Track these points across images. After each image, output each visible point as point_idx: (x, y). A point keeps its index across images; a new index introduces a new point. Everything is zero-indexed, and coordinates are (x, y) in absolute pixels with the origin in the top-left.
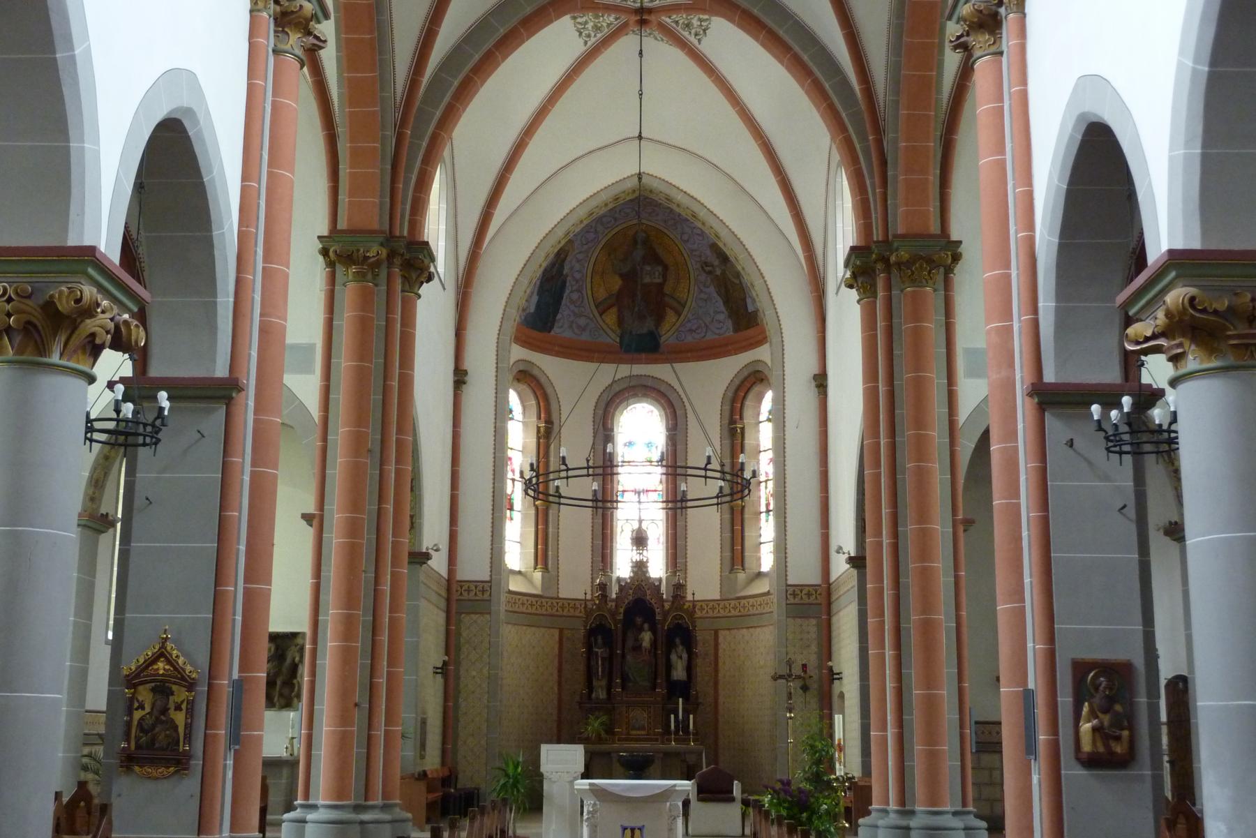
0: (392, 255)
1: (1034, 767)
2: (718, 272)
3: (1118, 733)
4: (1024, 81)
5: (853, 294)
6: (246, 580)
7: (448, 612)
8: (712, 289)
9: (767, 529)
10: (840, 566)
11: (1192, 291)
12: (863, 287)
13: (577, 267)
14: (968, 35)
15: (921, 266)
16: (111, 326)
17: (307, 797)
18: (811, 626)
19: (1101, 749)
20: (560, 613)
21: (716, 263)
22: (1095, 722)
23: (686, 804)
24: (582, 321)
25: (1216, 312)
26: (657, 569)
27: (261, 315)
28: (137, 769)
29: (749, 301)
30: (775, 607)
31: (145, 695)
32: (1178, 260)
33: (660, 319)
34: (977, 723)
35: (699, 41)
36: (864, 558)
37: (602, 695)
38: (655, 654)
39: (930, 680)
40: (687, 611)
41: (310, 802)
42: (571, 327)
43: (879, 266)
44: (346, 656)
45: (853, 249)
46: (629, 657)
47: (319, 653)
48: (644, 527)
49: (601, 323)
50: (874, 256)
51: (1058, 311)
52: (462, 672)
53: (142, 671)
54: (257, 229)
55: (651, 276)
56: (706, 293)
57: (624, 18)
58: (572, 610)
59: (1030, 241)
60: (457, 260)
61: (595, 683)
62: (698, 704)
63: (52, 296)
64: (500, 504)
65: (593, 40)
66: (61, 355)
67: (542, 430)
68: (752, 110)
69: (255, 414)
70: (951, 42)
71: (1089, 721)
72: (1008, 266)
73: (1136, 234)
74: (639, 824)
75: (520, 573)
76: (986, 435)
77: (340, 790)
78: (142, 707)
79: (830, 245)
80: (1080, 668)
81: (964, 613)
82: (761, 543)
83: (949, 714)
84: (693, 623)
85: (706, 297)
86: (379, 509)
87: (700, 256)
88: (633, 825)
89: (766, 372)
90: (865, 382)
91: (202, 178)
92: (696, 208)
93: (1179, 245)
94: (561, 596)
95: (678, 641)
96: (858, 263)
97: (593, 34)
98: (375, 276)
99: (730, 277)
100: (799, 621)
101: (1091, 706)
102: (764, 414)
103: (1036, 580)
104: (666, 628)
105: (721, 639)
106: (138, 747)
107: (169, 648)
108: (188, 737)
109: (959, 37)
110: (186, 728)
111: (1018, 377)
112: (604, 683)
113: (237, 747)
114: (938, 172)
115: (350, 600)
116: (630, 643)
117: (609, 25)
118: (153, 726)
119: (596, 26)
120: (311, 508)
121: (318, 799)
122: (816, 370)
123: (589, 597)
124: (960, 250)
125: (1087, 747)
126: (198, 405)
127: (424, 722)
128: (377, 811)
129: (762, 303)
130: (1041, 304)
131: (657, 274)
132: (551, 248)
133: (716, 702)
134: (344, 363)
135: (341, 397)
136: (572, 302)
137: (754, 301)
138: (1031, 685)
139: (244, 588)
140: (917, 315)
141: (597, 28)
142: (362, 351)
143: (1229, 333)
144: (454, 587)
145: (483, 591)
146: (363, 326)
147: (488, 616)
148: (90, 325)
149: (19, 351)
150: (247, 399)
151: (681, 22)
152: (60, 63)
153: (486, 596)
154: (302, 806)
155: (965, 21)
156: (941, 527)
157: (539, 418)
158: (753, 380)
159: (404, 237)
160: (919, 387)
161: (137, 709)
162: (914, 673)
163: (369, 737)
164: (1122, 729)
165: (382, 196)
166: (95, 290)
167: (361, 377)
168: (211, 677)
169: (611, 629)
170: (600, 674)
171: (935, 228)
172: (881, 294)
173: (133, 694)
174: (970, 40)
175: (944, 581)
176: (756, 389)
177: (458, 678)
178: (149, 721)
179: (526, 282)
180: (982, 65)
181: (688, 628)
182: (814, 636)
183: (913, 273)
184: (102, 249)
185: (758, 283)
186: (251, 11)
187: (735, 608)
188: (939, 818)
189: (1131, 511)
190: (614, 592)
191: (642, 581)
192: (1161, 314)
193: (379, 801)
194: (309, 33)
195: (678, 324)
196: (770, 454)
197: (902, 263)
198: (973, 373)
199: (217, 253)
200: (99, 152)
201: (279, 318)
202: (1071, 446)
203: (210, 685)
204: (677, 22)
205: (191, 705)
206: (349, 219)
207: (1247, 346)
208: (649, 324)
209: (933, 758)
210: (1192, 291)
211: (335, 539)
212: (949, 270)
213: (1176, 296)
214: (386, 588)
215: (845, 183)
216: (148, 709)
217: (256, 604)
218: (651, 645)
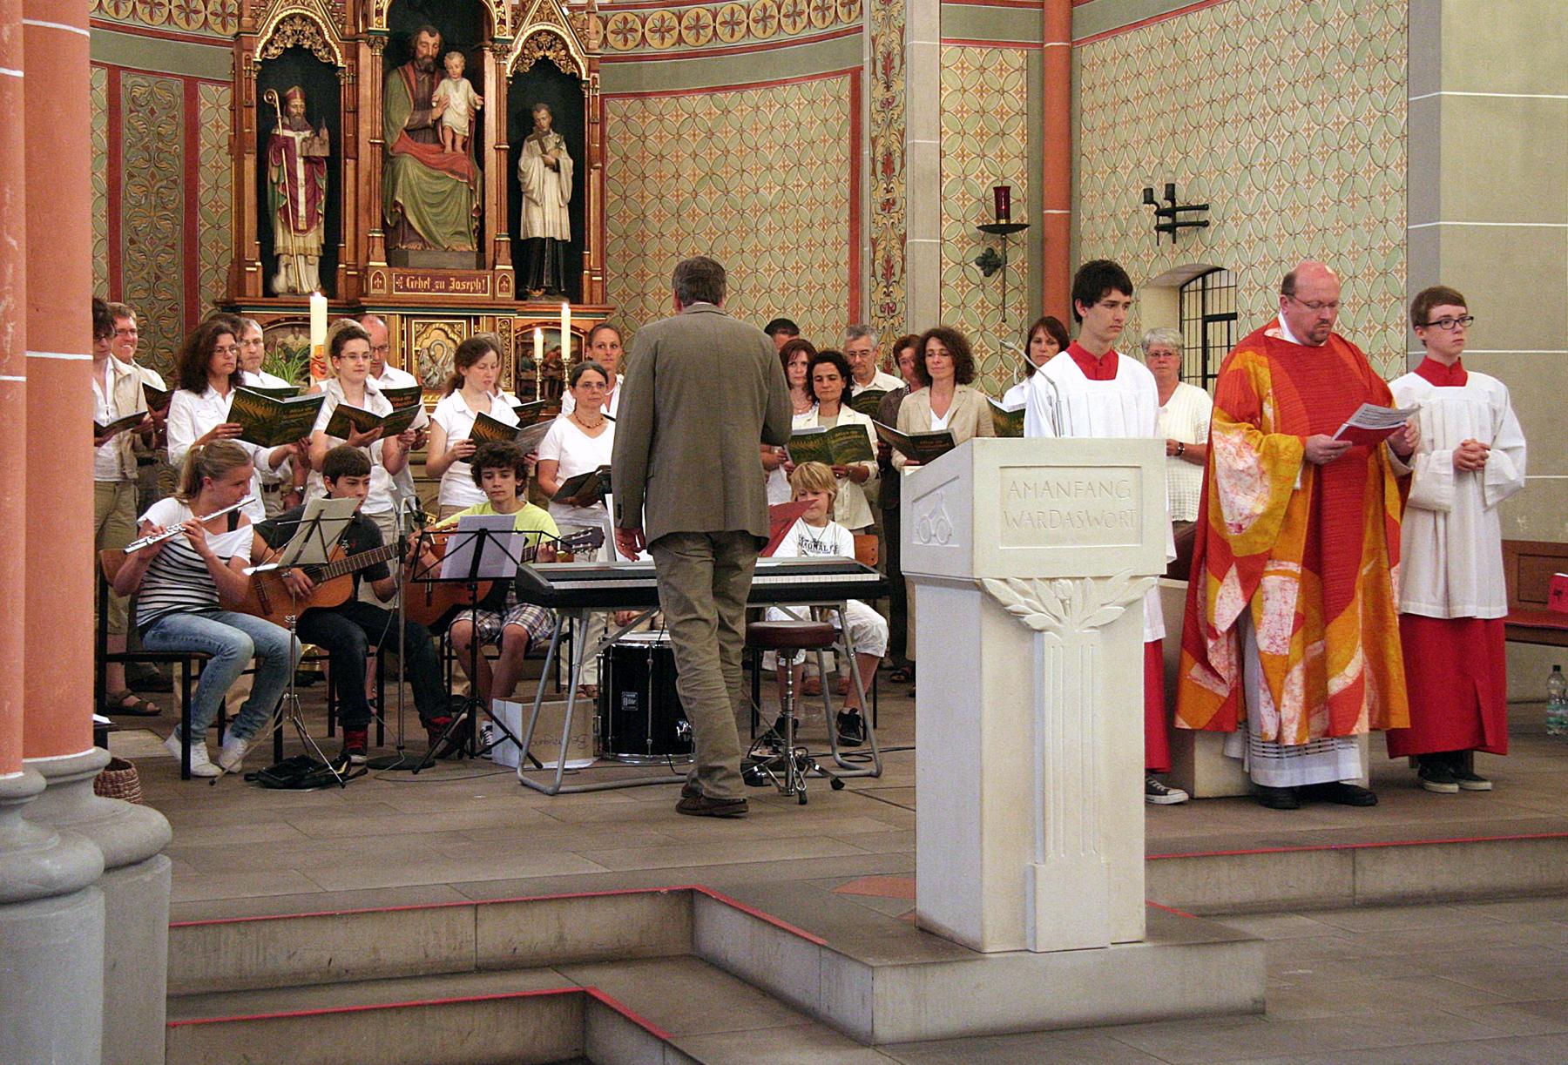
61: (282, 239)
95: (543, 116)
112: (313, 240)
182: (1015, 102)
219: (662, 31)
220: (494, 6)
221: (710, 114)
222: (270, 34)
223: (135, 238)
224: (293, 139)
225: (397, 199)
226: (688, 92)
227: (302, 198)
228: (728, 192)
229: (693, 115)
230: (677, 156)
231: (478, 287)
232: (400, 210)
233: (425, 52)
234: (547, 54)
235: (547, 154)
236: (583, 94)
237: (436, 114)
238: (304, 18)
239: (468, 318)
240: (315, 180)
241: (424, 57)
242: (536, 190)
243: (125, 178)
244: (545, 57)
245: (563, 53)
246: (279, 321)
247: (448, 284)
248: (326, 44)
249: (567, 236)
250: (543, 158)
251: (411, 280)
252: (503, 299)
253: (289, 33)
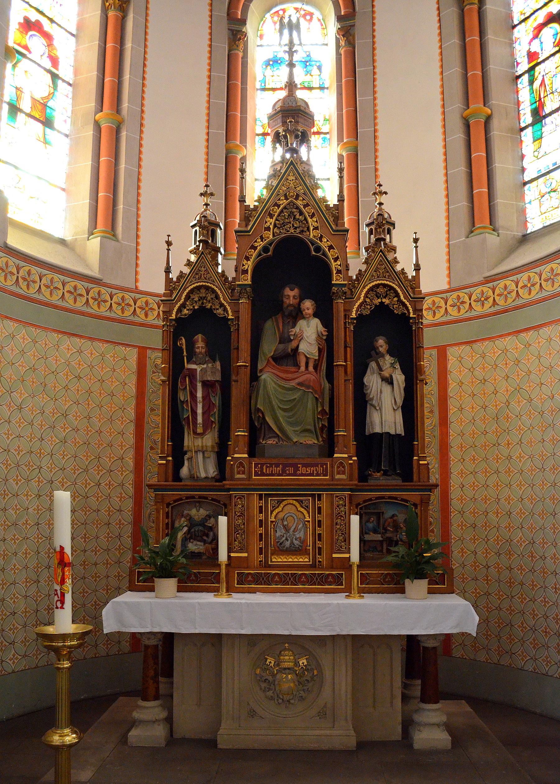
61: (188, 441)
75: (62, 242)
82: (525, 184)
84: (418, 311)
94: (142, 287)
95: (381, 343)
104: (354, 315)
169: (226, 319)
170: (200, 419)
181: (405, 318)
191: (297, 198)
218: (320, 350)
219: (482, 301)
220: (332, 261)
221: (517, 348)
222: (183, 300)
223: (154, 446)
224: (196, 370)
225: (258, 406)
226: (501, 336)
227: (200, 411)
228: (532, 400)
229: (505, 351)
230: (495, 380)
231: (320, 470)
232: (261, 415)
233: (288, 302)
234: (384, 300)
235: (382, 371)
236: (411, 327)
237: (294, 344)
238: (207, 288)
239: (313, 496)
240: (210, 398)
241: (288, 306)
242: (375, 398)
243: (148, 411)
244: (382, 303)
245: (396, 299)
246: (181, 499)
247: (296, 469)
248: (222, 305)
249: (400, 430)
250: (380, 374)
251: (267, 467)
252: (339, 480)
253: (196, 299)
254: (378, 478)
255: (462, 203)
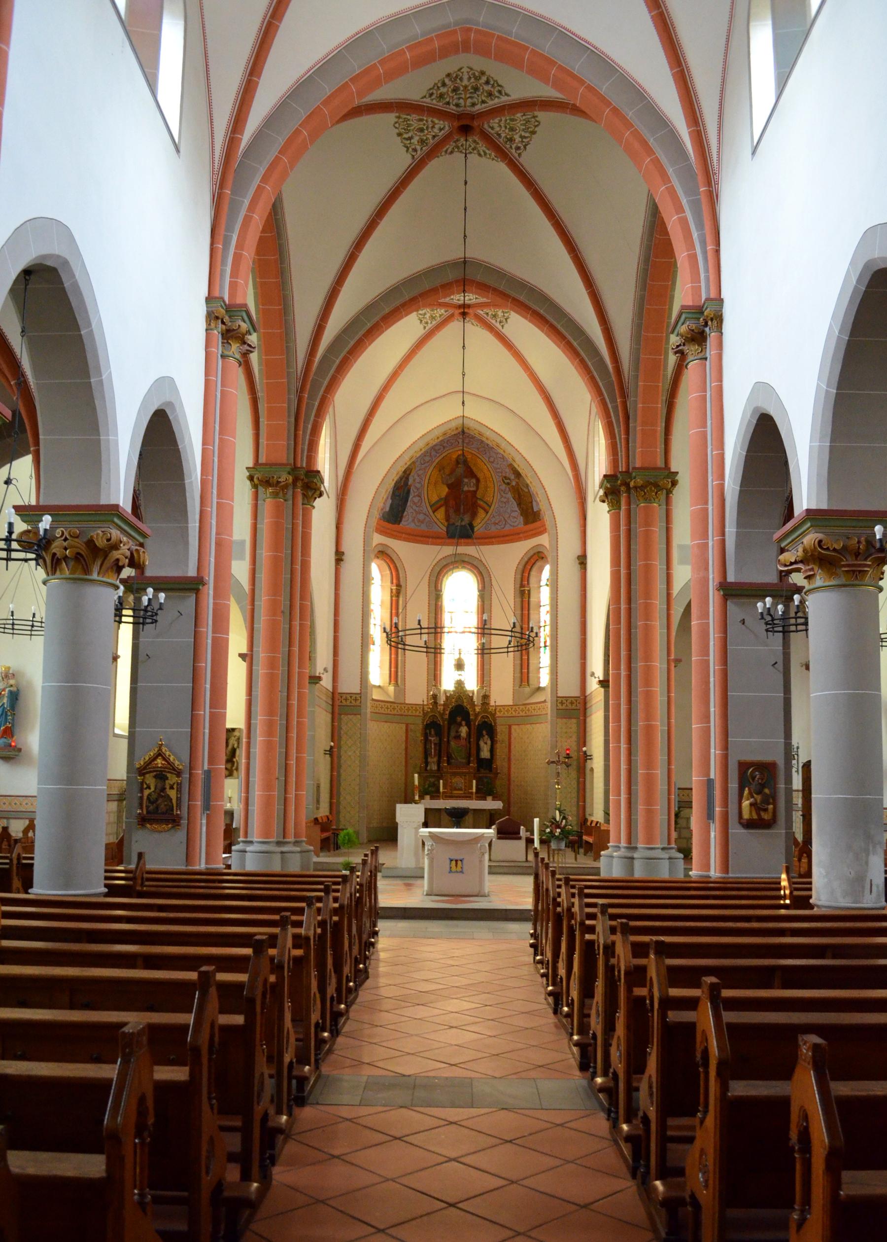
0: (295, 480)
1: (712, 826)
2: (514, 483)
3: (766, 807)
4: (720, 379)
5: (605, 507)
6: (211, 707)
7: (333, 713)
8: (509, 495)
9: (545, 658)
10: (593, 686)
11: (820, 536)
12: (612, 502)
13: (418, 480)
14: (684, 345)
15: (651, 489)
16: (128, 554)
17: (246, 835)
18: (573, 724)
19: (755, 817)
20: (406, 713)
21: (512, 477)
22: (752, 800)
23: (490, 845)
24: (421, 517)
25: (835, 550)
26: (472, 684)
27: (217, 534)
28: (148, 826)
29: (534, 503)
30: (548, 709)
31: (150, 780)
32: (810, 513)
33: (474, 515)
34: (679, 789)
35: (503, 326)
36: (608, 681)
37: (435, 767)
38: (470, 742)
39: (650, 764)
40: (491, 713)
41: (248, 839)
42: (413, 520)
43: (623, 488)
44: (269, 746)
45: (605, 476)
46: (452, 743)
47: (251, 745)
48: (462, 657)
49: (434, 517)
50: (619, 482)
51: (738, 534)
52: (342, 753)
53: (148, 765)
54: (213, 477)
55: (468, 486)
56: (505, 498)
57: (451, 311)
58: (414, 712)
59: (721, 488)
60: (337, 476)
61: (429, 759)
62: (498, 773)
63: (92, 537)
64: (365, 641)
65: (430, 325)
66: (98, 574)
67: (394, 591)
68: (538, 375)
69: (214, 599)
70: (673, 349)
71: (748, 799)
72: (706, 503)
73: (789, 489)
74: (461, 858)
75: (379, 687)
76: (689, 605)
77: (266, 832)
78: (149, 787)
79: (590, 464)
80: (743, 766)
81: (673, 721)
83: (661, 786)
84: (495, 720)
85: (505, 500)
86: (289, 651)
87: (502, 473)
88: (456, 858)
89: (545, 552)
90: (612, 566)
91: (178, 446)
92: (499, 440)
93: (814, 507)
94: (407, 702)
95: (484, 732)
96: (609, 486)
97: (429, 322)
98: (285, 494)
99: (522, 487)
100: (564, 720)
101: (749, 789)
102: (544, 582)
103: (717, 709)
105: (513, 730)
106: (148, 812)
107: (163, 750)
108: (179, 805)
109: (678, 346)
110: (177, 800)
111: (711, 577)
112: (435, 759)
113: (208, 812)
114: (664, 424)
115: (270, 710)
116: (453, 734)
117: (440, 316)
118: (157, 800)
119: (432, 316)
120: (244, 650)
121: (253, 837)
122: (579, 552)
123: (425, 703)
124: (677, 478)
125: (746, 815)
126: (177, 594)
127: (318, 787)
128: (291, 845)
129: (543, 506)
130: (727, 530)
131: (472, 484)
132: (401, 468)
133: (509, 775)
134: (264, 553)
135: (263, 576)
136: (415, 504)
137: (538, 504)
138: (712, 776)
139: (210, 712)
140: (648, 523)
141: (433, 318)
142: (276, 545)
143: (843, 563)
144: (337, 697)
145: (356, 700)
146: (277, 527)
147: (359, 716)
148: (116, 554)
149: (73, 572)
150: (209, 590)
151: (490, 314)
152: (93, 385)
153: (358, 703)
154: (244, 842)
155: (682, 336)
156: (659, 664)
157: (392, 583)
158: (536, 558)
159: (304, 468)
160: (648, 570)
161: (146, 789)
162: (640, 758)
163: (285, 799)
164: (769, 804)
165: (288, 439)
166: (119, 532)
167: (276, 562)
168: (191, 768)
171: (660, 463)
172: (623, 507)
173: (143, 780)
174: (685, 349)
175: (660, 700)
176: (538, 564)
177: (339, 757)
178: (154, 796)
179: (384, 491)
180: (693, 365)
181: (491, 724)
183: (645, 493)
184: (121, 505)
185: (540, 492)
186: (206, 330)
187: (522, 711)
188: (653, 851)
189: (780, 666)
190: (442, 700)
192: (800, 549)
193: (292, 839)
194: (244, 343)
195: (485, 520)
196: (548, 608)
197: (639, 487)
198: (682, 562)
199: (187, 494)
200: (118, 440)
201: (228, 536)
202: (743, 624)
203: (191, 774)
204: (487, 314)
205: (180, 785)
206: (267, 456)
207: (854, 571)
208: (467, 519)
209: (650, 814)
210: (820, 536)
211: (261, 671)
212: (669, 492)
213: (810, 539)
214: (295, 702)
215: (600, 426)
216: (153, 789)
217: (218, 717)
254: (482, 771)
255: (518, 675)
